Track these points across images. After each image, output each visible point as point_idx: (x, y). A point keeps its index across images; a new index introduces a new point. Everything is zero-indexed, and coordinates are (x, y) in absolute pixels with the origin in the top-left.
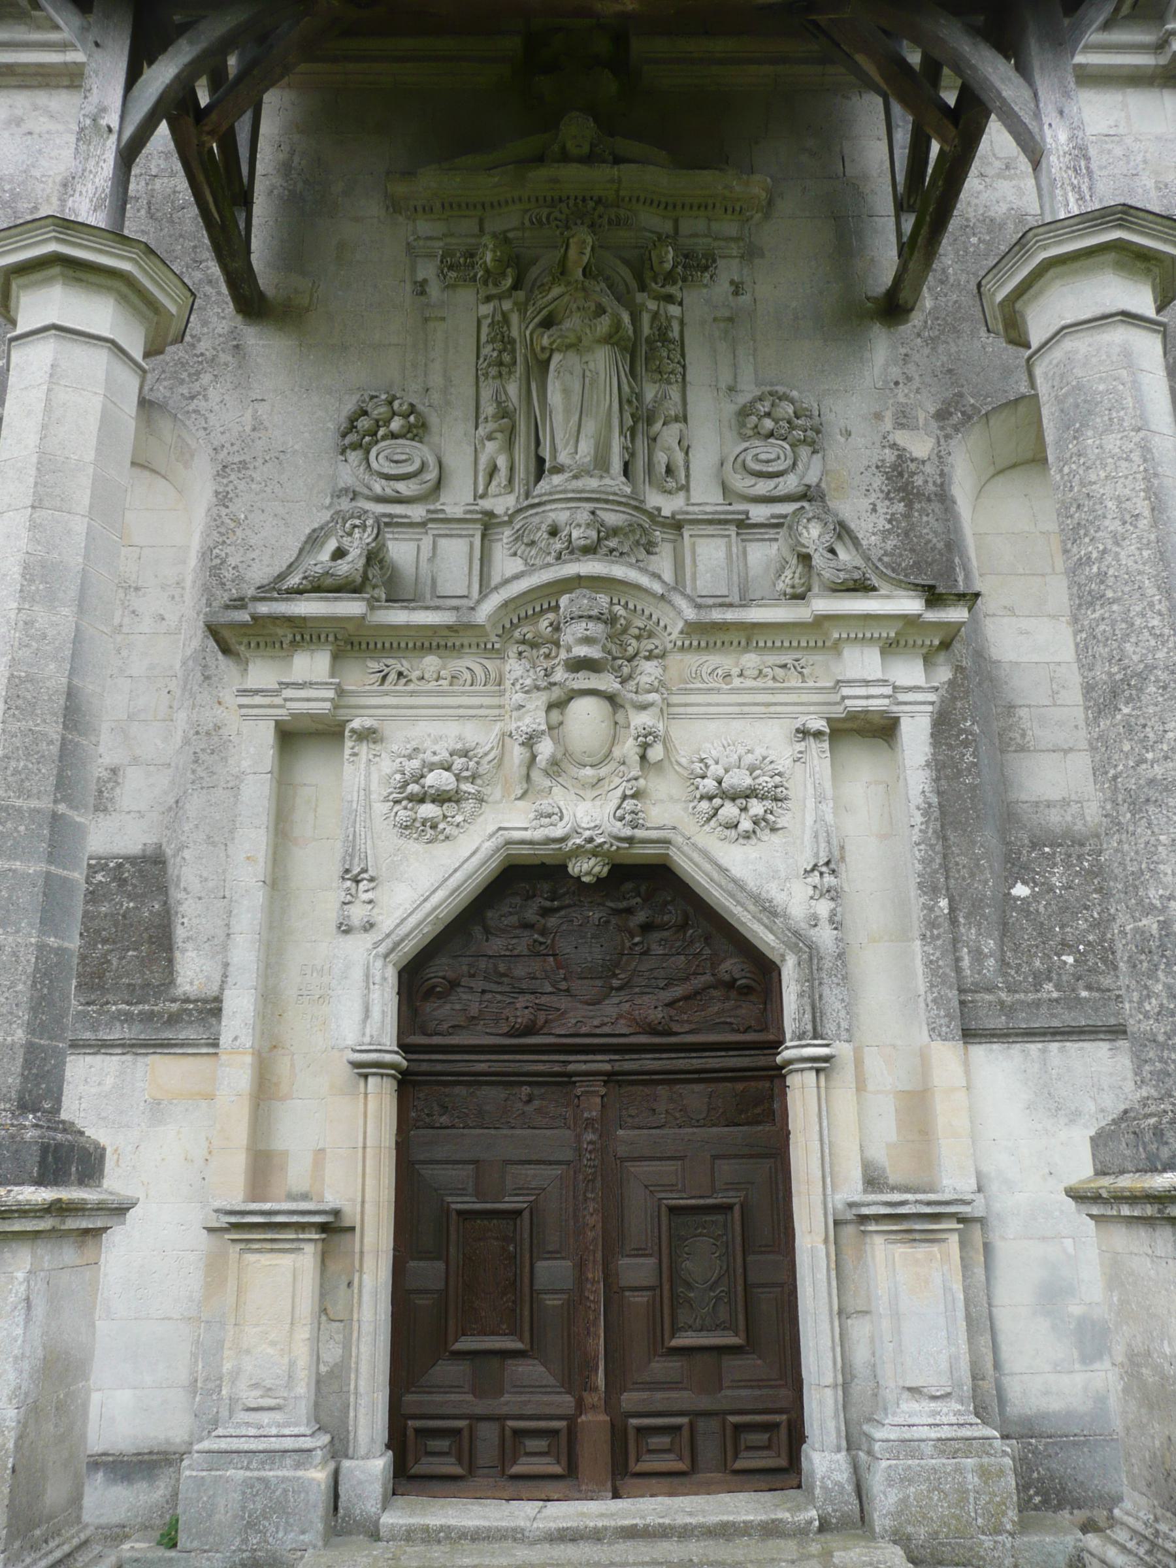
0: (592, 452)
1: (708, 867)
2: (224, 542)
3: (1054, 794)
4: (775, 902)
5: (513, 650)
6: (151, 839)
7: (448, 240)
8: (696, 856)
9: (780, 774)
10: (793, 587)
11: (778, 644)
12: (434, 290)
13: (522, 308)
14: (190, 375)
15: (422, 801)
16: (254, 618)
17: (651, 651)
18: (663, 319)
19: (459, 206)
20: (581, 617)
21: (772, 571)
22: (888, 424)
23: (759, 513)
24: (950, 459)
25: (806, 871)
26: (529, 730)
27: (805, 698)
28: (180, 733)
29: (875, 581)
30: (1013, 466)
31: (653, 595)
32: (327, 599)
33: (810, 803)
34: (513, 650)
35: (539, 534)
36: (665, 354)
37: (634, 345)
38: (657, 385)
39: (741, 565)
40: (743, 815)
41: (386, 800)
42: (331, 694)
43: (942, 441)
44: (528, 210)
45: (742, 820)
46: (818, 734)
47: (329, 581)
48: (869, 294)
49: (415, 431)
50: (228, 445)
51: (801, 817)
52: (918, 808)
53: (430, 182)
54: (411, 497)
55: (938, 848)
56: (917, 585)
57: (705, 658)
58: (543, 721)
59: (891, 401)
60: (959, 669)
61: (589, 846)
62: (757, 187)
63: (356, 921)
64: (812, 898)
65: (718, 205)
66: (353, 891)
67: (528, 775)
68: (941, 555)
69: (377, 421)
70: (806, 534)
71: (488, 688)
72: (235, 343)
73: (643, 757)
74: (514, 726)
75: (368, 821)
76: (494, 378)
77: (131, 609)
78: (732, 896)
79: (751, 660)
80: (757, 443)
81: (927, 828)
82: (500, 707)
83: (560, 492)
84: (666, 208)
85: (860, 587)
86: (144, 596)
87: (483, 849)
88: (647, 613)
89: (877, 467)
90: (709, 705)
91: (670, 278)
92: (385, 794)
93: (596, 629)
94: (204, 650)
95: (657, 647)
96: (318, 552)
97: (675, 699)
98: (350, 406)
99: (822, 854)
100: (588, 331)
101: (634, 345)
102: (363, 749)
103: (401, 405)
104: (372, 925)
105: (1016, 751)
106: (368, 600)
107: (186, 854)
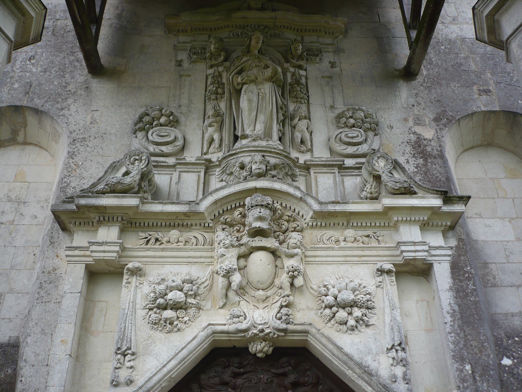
0: (263, 129)
1: (331, 346)
2: (70, 175)
3: (515, 309)
4: (371, 368)
5: (219, 227)
6: (14, 334)
7: (194, 43)
8: (324, 340)
9: (369, 294)
10: (371, 193)
11: (364, 224)
12: (186, 64)
13: (227, 69)
14: (62, 99)
15: (165, 309)
16: (78, 206)
17: (295, 228)
18: (297, 75)
19: (200, 30)
20: (257, 205)
21: (358, 189)
22: (411, 123)
23: (349, 162)
24: (443, 139)
25: (387, 349)
26: (228, 268)
27: (380, 253)
28: (36, 274)
29: (416, 190)
30: (472, 148)
31: (295, 197)
32: (118, 197)
33: (387, 310)
34: (219, 227)
35: (235, 168)
36: (299, 89)
37: (284, 85)
38: (295, 104)
39: (341, 187)
40: (350, 317)
41: (144, 308)
42: (117, 248)
43: (438, 131)
44: (232, 31)
45: (349, 320)
46: (389, 272)
47: (119, 187)
48: (396, 68)
49: (172, 123)
50: (77, 130)
51: (383, 318)
52: (448, 313)
53: (186, 19)
54: (167, 153)
55: (462, 335)
56: (438, 191)
57: (325, 232)
58: (235, 263)
59: (411, 113)
60: (460, 240)
61: (261, 334)
62: (340, 22)
63: (122, 379)
64: (392, 365)
65: (322, 30)
66: (122, 361)
67: (226, 295)
68: (444, 183)
69: (153, 118)
70: (377, 165)
71: (205, 247)
72: (86, 86)
73: (292, 285)
74: (219, 266)
75: (133, 319)
76: (213, 100)
77: (20, 212)
78: (345, 363)
79: (350, 233)
80: (346, 129)
81: (454, 324)
82: (212, 257)
83: (246, 147)
84: (297, 31)
85: (408, 192)
86: (28, 206)
87: (199, 336)
88: (292, 208)
89: (407, 142)
90: (328, 256)
91: (300, 57)
92: (144, 305)
93: (265, 212)
94: (52, 229)
95: (298, 226)
96: (115, 174)
97: (309, 253)
98: (142, 110)
99: (396, 339)
100: (261, 74)
101: (284, 85)
102: (134, 280)
103: (166, 111)
104: (131, 382)
105: (492, 287)
106: (140, 197)
107: (29, 340)
